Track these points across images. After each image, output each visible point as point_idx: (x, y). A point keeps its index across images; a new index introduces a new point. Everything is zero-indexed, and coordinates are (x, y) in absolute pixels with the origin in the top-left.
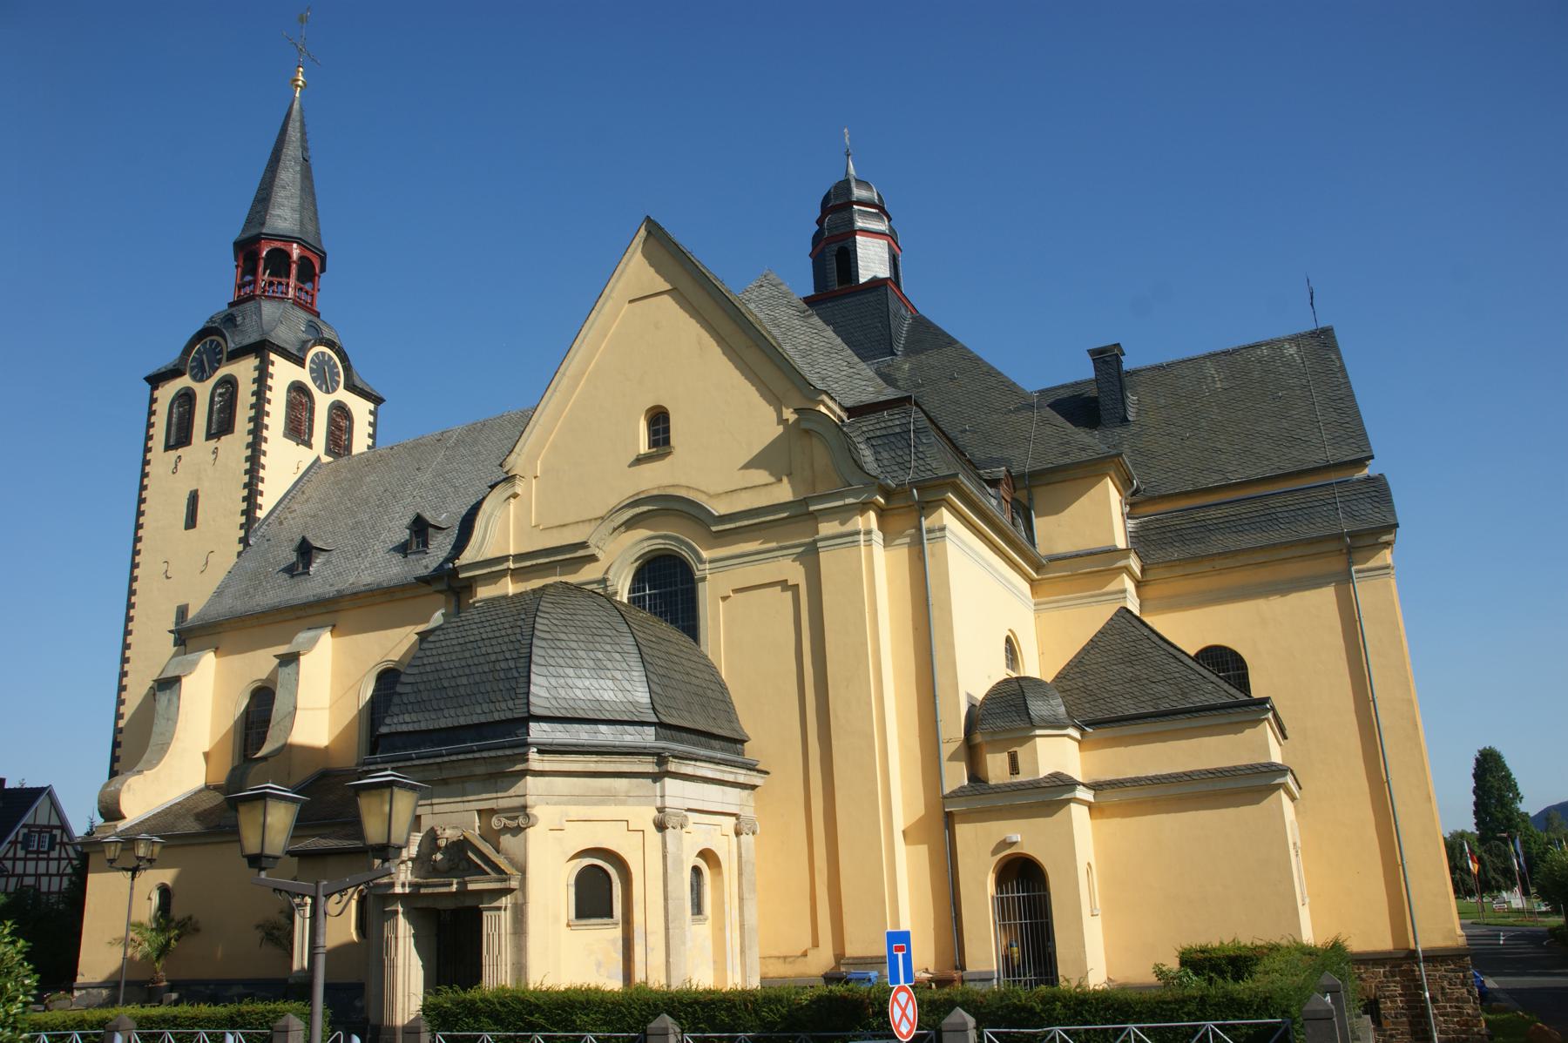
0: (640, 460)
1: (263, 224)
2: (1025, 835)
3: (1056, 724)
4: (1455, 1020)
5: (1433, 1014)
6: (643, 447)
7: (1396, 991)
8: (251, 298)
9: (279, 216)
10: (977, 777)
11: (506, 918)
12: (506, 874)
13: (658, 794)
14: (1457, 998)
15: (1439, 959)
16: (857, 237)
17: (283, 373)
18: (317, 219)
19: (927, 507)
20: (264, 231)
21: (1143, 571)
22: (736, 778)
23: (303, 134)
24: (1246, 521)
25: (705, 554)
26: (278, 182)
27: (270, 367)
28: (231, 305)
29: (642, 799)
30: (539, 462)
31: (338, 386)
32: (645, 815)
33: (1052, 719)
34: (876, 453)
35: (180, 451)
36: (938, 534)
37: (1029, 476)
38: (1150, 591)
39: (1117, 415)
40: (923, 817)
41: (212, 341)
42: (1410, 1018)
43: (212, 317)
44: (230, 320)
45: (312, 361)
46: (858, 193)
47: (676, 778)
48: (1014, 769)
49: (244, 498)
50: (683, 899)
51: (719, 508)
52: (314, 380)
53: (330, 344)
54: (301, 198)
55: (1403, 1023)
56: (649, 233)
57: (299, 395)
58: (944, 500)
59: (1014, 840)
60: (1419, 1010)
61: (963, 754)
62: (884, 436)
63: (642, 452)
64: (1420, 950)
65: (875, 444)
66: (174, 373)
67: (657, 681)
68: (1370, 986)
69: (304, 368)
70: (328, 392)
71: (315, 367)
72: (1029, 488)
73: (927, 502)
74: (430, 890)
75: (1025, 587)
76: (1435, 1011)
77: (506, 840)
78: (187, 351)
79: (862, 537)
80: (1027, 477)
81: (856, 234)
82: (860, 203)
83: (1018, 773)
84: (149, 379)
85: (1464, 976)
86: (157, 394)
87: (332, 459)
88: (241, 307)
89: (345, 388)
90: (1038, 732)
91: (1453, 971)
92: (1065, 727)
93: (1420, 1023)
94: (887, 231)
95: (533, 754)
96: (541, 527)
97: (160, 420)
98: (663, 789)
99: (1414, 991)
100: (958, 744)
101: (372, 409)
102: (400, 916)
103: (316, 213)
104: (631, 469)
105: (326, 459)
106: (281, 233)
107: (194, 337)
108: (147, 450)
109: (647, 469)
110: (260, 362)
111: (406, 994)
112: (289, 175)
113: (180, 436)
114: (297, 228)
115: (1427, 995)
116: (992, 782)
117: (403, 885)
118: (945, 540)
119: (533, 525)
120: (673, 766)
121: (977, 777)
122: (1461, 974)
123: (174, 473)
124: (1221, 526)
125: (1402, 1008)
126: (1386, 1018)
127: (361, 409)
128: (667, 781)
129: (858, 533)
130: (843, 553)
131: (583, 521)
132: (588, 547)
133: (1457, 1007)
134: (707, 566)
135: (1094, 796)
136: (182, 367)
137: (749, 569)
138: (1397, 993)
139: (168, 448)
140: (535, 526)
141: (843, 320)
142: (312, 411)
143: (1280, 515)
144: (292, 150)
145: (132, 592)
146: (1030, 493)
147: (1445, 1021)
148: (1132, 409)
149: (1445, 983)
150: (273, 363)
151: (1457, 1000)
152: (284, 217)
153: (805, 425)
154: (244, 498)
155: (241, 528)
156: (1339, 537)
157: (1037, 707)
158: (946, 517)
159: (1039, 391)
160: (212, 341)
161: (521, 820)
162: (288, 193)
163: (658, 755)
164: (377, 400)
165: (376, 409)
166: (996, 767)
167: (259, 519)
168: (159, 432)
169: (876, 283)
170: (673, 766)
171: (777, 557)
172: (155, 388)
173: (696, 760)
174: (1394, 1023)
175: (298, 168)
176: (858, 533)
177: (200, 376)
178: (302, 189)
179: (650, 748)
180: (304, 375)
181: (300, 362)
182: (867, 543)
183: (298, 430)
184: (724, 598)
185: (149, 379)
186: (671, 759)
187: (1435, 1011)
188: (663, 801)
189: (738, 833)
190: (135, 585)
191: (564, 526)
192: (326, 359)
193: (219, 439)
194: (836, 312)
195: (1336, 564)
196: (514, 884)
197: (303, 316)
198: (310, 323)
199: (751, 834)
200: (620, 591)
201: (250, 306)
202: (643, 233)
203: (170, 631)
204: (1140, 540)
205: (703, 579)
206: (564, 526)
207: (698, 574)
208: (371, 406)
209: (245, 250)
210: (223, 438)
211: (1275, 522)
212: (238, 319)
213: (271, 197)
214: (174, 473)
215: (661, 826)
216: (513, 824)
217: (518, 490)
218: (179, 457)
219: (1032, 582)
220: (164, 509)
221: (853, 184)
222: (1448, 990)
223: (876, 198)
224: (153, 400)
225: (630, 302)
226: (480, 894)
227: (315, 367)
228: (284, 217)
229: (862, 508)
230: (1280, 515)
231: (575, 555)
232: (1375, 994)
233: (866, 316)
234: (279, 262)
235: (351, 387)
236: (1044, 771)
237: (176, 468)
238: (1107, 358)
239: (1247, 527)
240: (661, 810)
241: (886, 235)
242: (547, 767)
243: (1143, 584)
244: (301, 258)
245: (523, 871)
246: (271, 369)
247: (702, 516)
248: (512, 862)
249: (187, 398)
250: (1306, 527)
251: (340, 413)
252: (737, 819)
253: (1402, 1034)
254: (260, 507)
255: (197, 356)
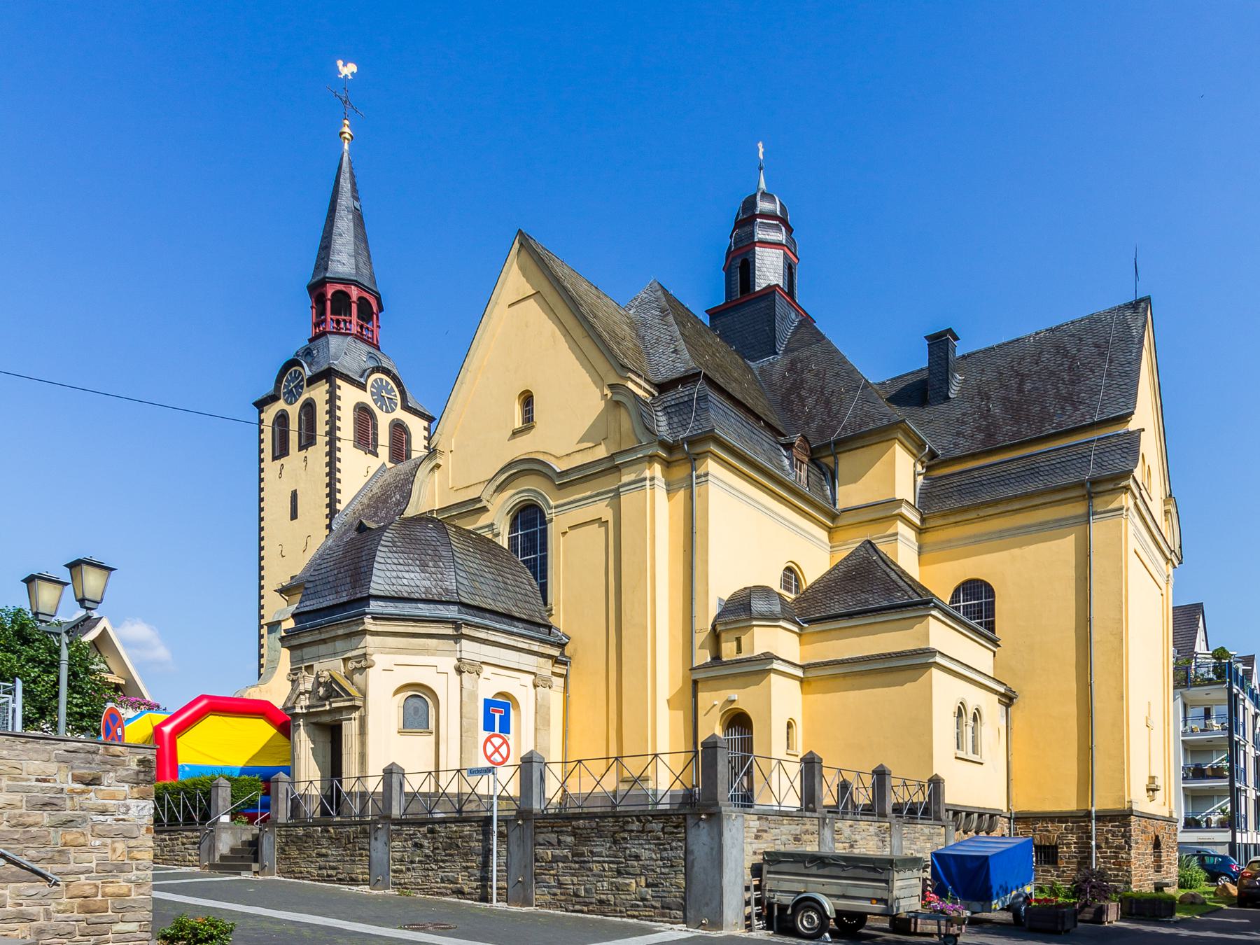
0: (516, 433)
1: (326, 269)
2: (743, 698)
3: (771, 618)
4: (1112, 861)
5: (1096, 857)
6: (518, 423)
7: (1071, 840)
8: (324, 334)
9: (339, 261)
10: (717, 657)
11: (355, 725)
12: (352, 696)
13: (458, 650)
14: (1116, 846)
15: (1108, 818)
16: (756, 248)
17: (349, 396)
18: (371, 263)
19: (694, 459)
20: (327, 275)
21: (923, 520)
22: (529, 647)
23: (354, 185)
24: (1013, 476)
25: (552, 503)
26: (336, 230)
27: (337, 390)
28: (311, 340)
29: (450, 652)
30: (453, 440)
31: (396, 406)
32: (449, 663)
33: (768, 614)
34: (670, 418)
35: (283, 461)
36: (703, 479)
37: (835, 445)
38: (930, 537)
39: (941, 394)
40: (682, 687)
41: (295, 371)
42: (1079, 860)
43: (298, 352)
44: (308, 352)
45: (373, 386)
46: (763, 206)
47: (473, 641)
48: (739, 650)
49: (327, 494)
50: (477, 720)
51: (559, 466)
52: (375, 402)
53: (387, 372)
54: (355, 244)
55: (1073, 862)
56: (521, 244)
57: (364, 415)
58: (710, 452)
59: (733, 698)
60: (1086, 854)
61: (708, 643)
62: (677, 404)
63: (517, 427)
64: (1093, 811)
65: (669, 411)
66: (273, 398)
67: (465, 576)
68: (1054, 836)
69: (366, 391)
70: (387, 412)
71: (375, 391)
72: (835, 455)
73: (698, 454)
74: (315, 710)
75: (823, 535)
76: (1098, 855)
77: (357, 677)
78: (279, 381)
79: (648, 483)
80: (832, 445)
81: (756, 246)
82: (763, 215)
83: (741, 653)
84: (255, 404)
85: (1125, 830)
86: (263, 416)
87: (394, 465)
88: (316, 342)
89: (402, 409)
90: (755, 623)
91: (1117, 826)
92: (778, 619)
93: (1086, 863)
94: (784, 242)
95: (368, 619)
96: (455, 489)
97: (267, 436)
98: (461, 646)
99: (1085, 840)
100: (706, 633)
101: (427, 426)
102: (302, 727)
103: (369, 256)
104: (511, 441)
105: (389, 465)
106: (341, 276)
107: (280, 371)
108: (261, 460)
109: (521, 440)
110: (330, 386)
111: (307, 775)
112: (344, 224)
113: (281, 450)
114: (353, 272)
115: (1093, 843)
116: (724, 659)
117: (302, 708)
118: (707, 484)
119: (450, 487)
120: (465, 631)
121: (717, 657)
122: (1123, 829)
123: (280, 478)
124: (993, 480)
125: (1075, 852)
126: (1062, 859)
127: (416, 426)
128: (464, 642)
129: (645, 479)
130: (635, 494)
131: (480, 483)
132: (481, 501)
133: (1114, 852)
134: (554, 511)
135: (803, 673)
136: (277, 394)
137: (579, 510)
138: (1072, 842)
139: (274, 458)
140: (451, 488)
141: (741, 325)
142: (375, 427)
143: (1041, 469)
144: (345, 200)
145: (261, 568)
146: (836, 458)
147: (1104, 862)
148: (954, 387)
149: (1110, 835)
150: (339, 388)
151: (1116, 847)
152: (343, 262)
153: (617, 398)
154: (327, 494)
155: (327, 518)
156: (1081, 485)
157: (758, 606)
158: (711, 466)
159: (891, 380)
160: (295, 371)
161: (363, 663)
162: (344, 241)
163: (454, 623)
164: (430, 419)
165: (429, 426)
166: (728, 650)
167: (339, 511)
168: (267, 446)
169: (771, 290)
170: (465, 631)
171: (596, 501)
172: (261, 412)
173: (488, 629)
174: (1067, 863)
175: (351, 217)
176: (645, 479)
177: (292, 397)
178: (355, 237)
179: (451, 618)
180: (366, 398)
181: (363, 387)
182: (652, 487)
183: (366, 440)
184: (564, 533)
185: (255, 404)
186: (463, 625)
187: (1098, 855)
188: (461, 655)
189: (535, 686)
190: (263, 563)
191: (468, 487)
192: (384, 384)
193: (307, 450)
194: (736, 319)
195: (1078, 509)
196: (358, 703)
197: (365, 348)
198: (370, 355)
199: (548, 688)
200: (501, 532)
201: (323, 340)
202: (517, 245)
203: (276, 591)
204: (929, 499)
205: (551, 520)
206: (468, 487)
207: (548, 517)
208: (426, 424)
209: (316, 290)
210: (309, 448)
211: (1036, 475)
212: (314, 352)
213: (330, 246)
214: (280, 478)
215: (459, 671)
216: (359, 666)
217: (439, 461)
218: (282, 465)
219: (830, 530)
220: (276, 507)
221: (758, 198)
222: (1110, 840)
223: (778, 209)
224: (261, 421)
225: (510, 306)
226: (339, 710)
227: (375, 391)
228: (343, 262)
229: (651, 459)
230: (1041, 469)
231: (474, 507)
232: (1056, 842)
233: (758, 321)
234: (342, 302)
235: (406, 407)
236: (758, 651)
237: (281, 473)
238: (940, 343)
239: (1013, 481)
240: (459, 660)
241: (782, 245)
242: (380, 629)
243: (924, 531)
244: (360, 299)
245: (365, 696)
246: (338, 392)
247: (550, 473)
248: (359, 690)
249: (282, 418)
250: (1060, 478)
251: (399, 429)
252: (535, 676)
253: (1072, 870)
254: (339, 502)
255: (286, 384)
